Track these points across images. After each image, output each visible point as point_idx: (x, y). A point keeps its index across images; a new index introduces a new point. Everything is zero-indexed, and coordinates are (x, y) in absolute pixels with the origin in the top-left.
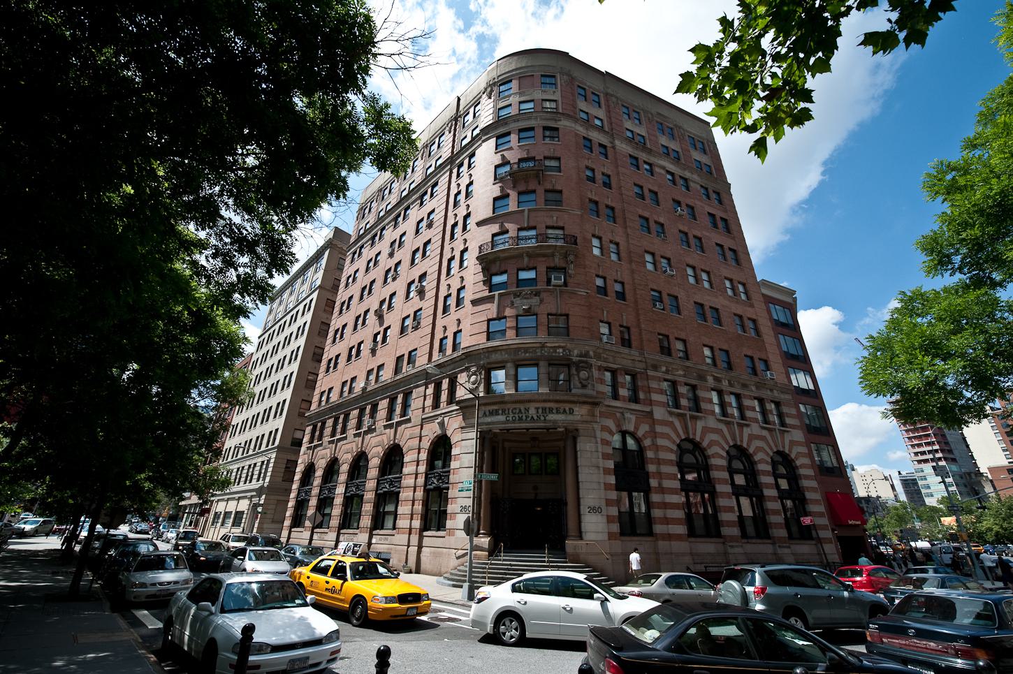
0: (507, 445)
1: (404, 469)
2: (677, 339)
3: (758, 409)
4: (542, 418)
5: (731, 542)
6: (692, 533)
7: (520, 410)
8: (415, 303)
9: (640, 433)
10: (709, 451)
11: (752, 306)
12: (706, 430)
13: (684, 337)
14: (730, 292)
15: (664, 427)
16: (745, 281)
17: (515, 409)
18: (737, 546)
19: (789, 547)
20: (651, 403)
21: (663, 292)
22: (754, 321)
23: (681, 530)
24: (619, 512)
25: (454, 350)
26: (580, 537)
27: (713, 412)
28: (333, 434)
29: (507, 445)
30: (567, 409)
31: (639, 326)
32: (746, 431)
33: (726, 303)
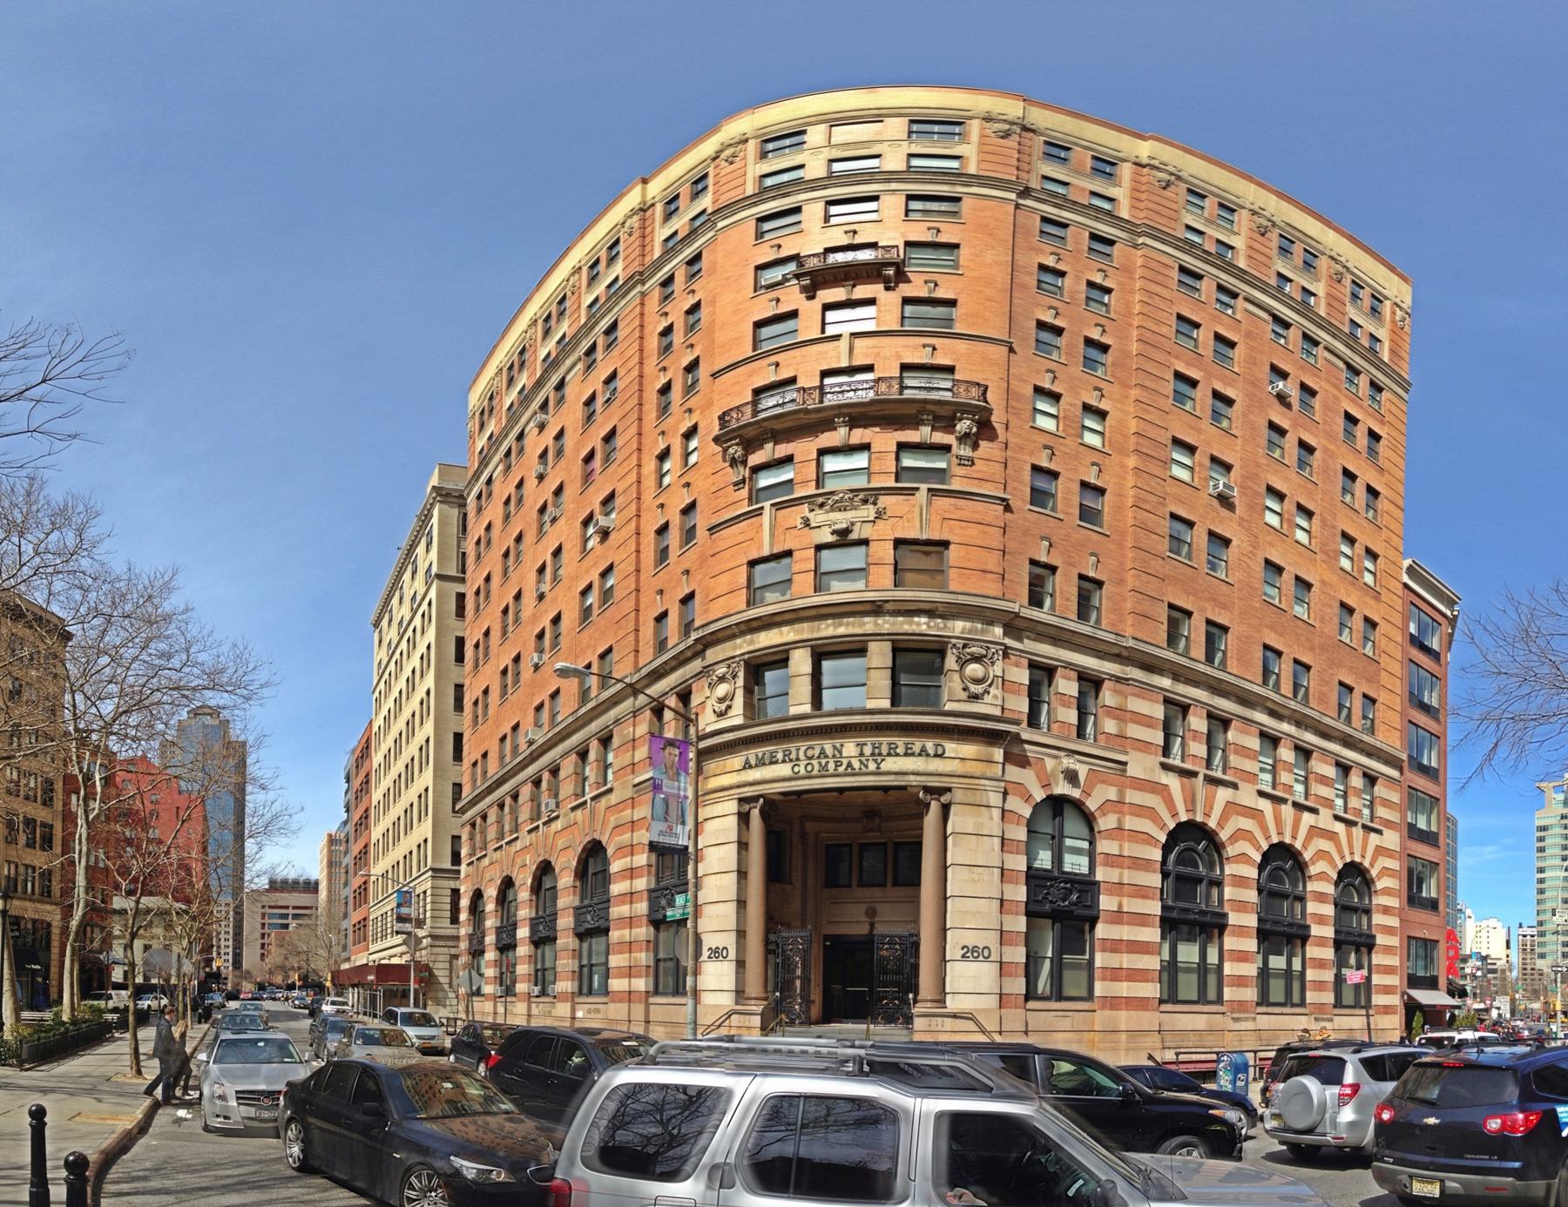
0: (810, 827)
6: (1171, 996)
8: (601, 555)
12: (1232, 808)
18: (1246, 1019)
23: (1152, 990)
24: (1029, 868)
28: (501, 836)
29: (810, 827)
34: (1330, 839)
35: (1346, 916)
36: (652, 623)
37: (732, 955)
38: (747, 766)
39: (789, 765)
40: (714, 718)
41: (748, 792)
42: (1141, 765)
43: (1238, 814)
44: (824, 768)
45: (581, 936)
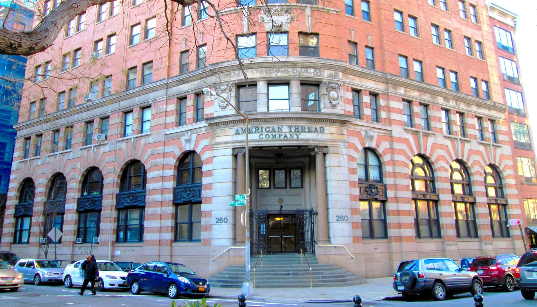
1: (147, 185)
2: (414, 60)
3: (477, 127)
4: (295, 137)
5: (448, 241)
7: (273, 129)
9: (380, 150)
10: (436, 165)
11: (480, 29)
12: (435, 146)
13: (421, 59)
14: (462, 15)
15: (401, 144)
16: (475, 4)
17: (268, 127)
18: (453, 245)
19: (492, 244)
20: (390, 121)
21: (404, 12)
22: (480, 43)
23: (411, 232)
25: (198, 66)
26: (328, 239)
27: (441, 130)
30: (318, 128)
31: (381, 47)
32: (467, 146)
33: (458, 25)
35: (88, 82)
36: (179, 54)
37: (230, 220)
38: (237, 133)
40: (219, 109)
41: (238, 145)
45: (119, 209)
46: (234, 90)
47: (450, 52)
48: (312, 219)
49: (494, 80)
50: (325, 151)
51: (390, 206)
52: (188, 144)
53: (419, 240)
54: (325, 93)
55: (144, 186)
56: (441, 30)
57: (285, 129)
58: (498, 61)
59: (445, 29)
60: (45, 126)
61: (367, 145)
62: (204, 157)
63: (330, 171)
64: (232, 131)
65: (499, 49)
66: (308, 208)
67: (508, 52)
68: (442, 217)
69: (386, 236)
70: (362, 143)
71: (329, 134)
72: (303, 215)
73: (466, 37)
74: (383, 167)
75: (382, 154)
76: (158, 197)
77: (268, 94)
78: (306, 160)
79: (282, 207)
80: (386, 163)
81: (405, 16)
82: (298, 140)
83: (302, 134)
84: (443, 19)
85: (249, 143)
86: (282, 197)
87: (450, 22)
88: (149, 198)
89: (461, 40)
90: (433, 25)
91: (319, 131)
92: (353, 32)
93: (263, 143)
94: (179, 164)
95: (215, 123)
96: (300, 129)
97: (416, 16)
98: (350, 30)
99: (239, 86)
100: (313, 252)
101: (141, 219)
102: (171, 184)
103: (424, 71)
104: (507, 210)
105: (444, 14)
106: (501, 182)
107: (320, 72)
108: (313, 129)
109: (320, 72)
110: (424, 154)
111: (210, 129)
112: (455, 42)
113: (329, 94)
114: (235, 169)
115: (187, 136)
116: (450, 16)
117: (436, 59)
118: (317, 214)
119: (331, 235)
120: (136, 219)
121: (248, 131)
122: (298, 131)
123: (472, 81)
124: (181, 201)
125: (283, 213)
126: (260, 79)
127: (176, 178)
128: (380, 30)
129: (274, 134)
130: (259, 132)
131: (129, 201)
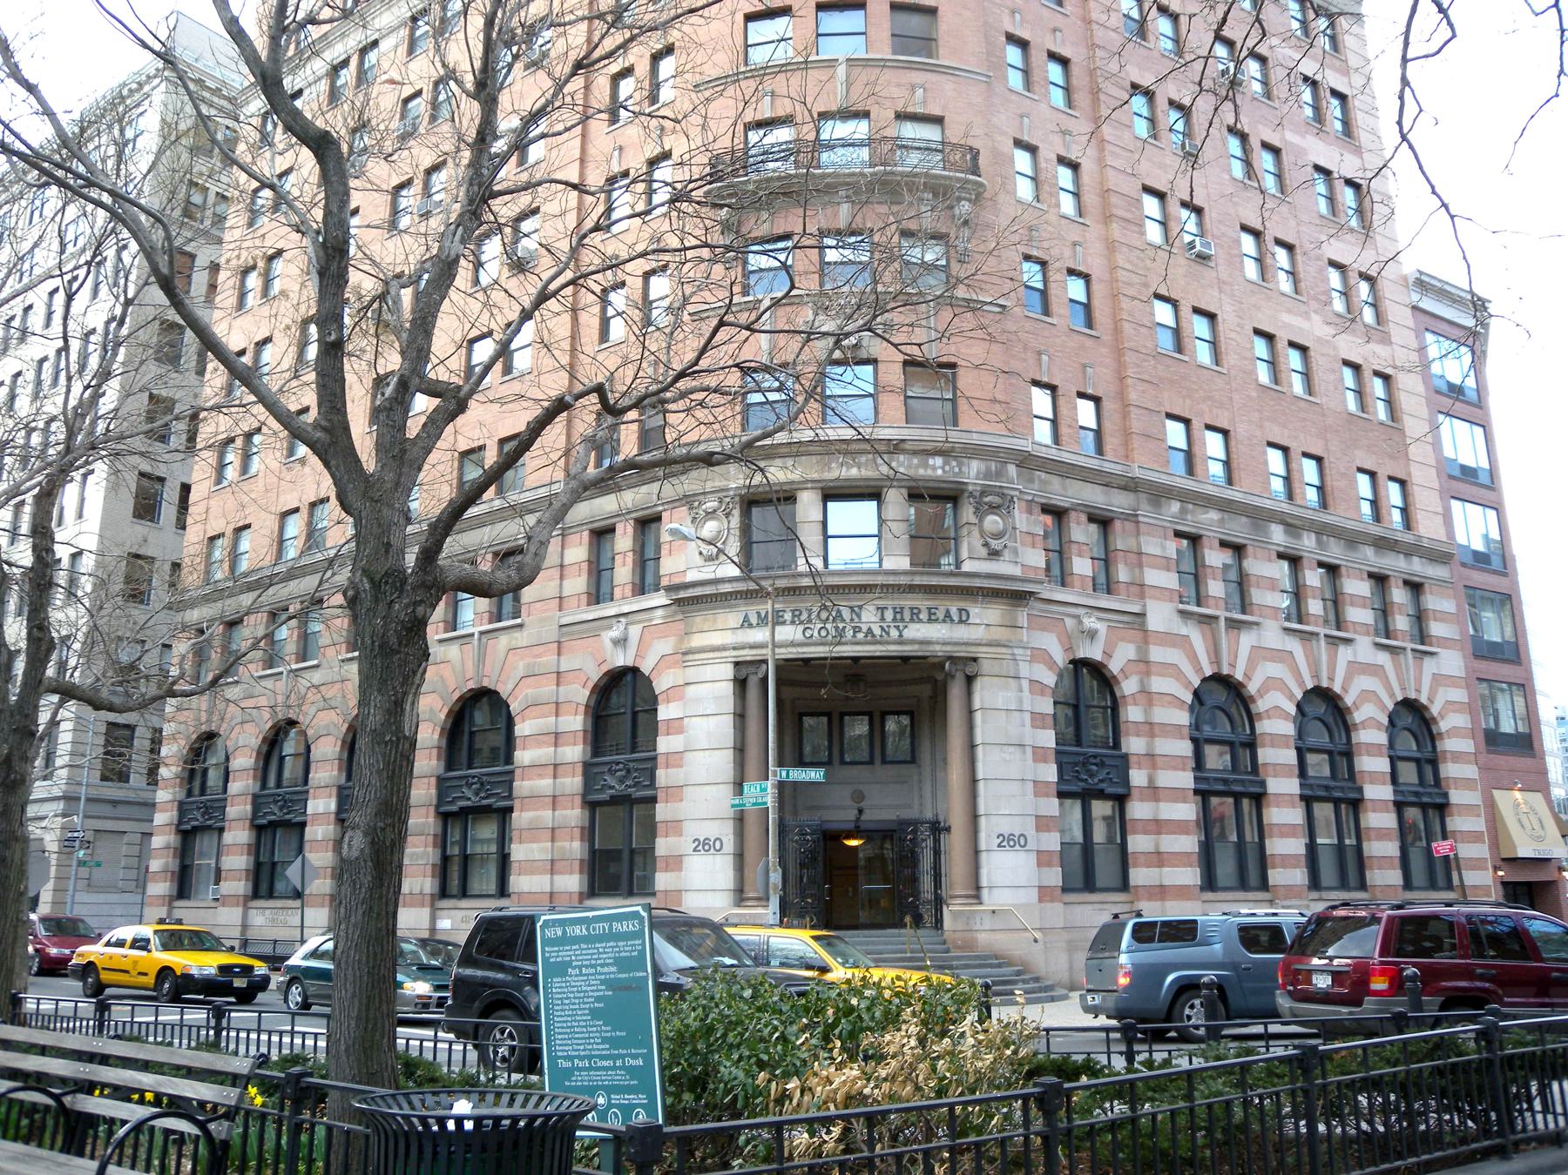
2: (1209, 427)
4: (894, 633)
11: (1386, 339)
13: (1225, 426)
14: (1339, 305)
26: (976, 892)
30: (954, 611)
31: (1121, 395)
34: (1374, 674)
37: (729, 845)
38: (746, 623)
39: (801, 628)
40: (699, 561)
41: (748, 655)
42: (1161, 616)
43: (1265, 659)
44: (841, 633)
45: (445, 817)
46: (736, 512)
47: (1302, 404)
48: (937, 841)
49: (1425, 481)
50: (970, 670)
51: (1138, 810)
52: (620, 651)
53: (1209, 895)
54: (973, 519)
55: (509, 759)
56: (1281, 345)
57: (869, 616)
58: (1436, 428)
59: (1292, 344)
60: (246, 599)
61: (1081, 654)
62: (660, 685)
63: (984, 721)
64: (733, 618)
65: (1438, 392)
66: (929, 815)
67: (1464, 402)
68: (1369, 840)
69: (1124, 886)
70: (1069, 649)
71: (984, 621)
72: (914, 832)
73: (1346, 363)
74: (1122, 710)
75: (1120, 677)
76: (544, 784)
77: (824, 524)
78: (925, 690)
79: (861, 811)
80: (1129, 700)
81: (1186, 311)
82: (901, 641)
83: (913, 626)
84: (1286, 318)
85: (777, 650)
86: (861, 787)
87: (1305, 325)
88: (522, 786)
89: (1333, 371)
90: (1258, 332)
91: (956, 618)
92: (1045, 358)
93: (812, 649)
94: (598, 703)
95: (692, 601)
96: (907, 616)
97: (1212, 309)
98: (1039, 353)
99: (750, 502)
100: (938, 923)
101: (503, 839)
102: (575, 752)
103: (1234, 456)
104: (1448, 820)
105: (1289, 303)
106: (1434, 747)
107: (960, 465)
108: (941, 615)
109: (960, 465)
110: (1229, 676)
111: (675, 613)
112: (1319, 376)
113: (981, 520)
114: (740, 716)
115: (615, 632)
116: (1303, 308)
117: (1267, 424)
118: (948, 829)
119: (984, 882)
120: (489, 841)
121: (778, 620)
122: (902, 620)
123: (1363, 481)
124: (604, 797)
125: (863, 827)
126: (803, 485)
127: (589, 736)
128: (1119, 352)
129: (841, 625)
130: (801, 623)
131: (469, 794)
